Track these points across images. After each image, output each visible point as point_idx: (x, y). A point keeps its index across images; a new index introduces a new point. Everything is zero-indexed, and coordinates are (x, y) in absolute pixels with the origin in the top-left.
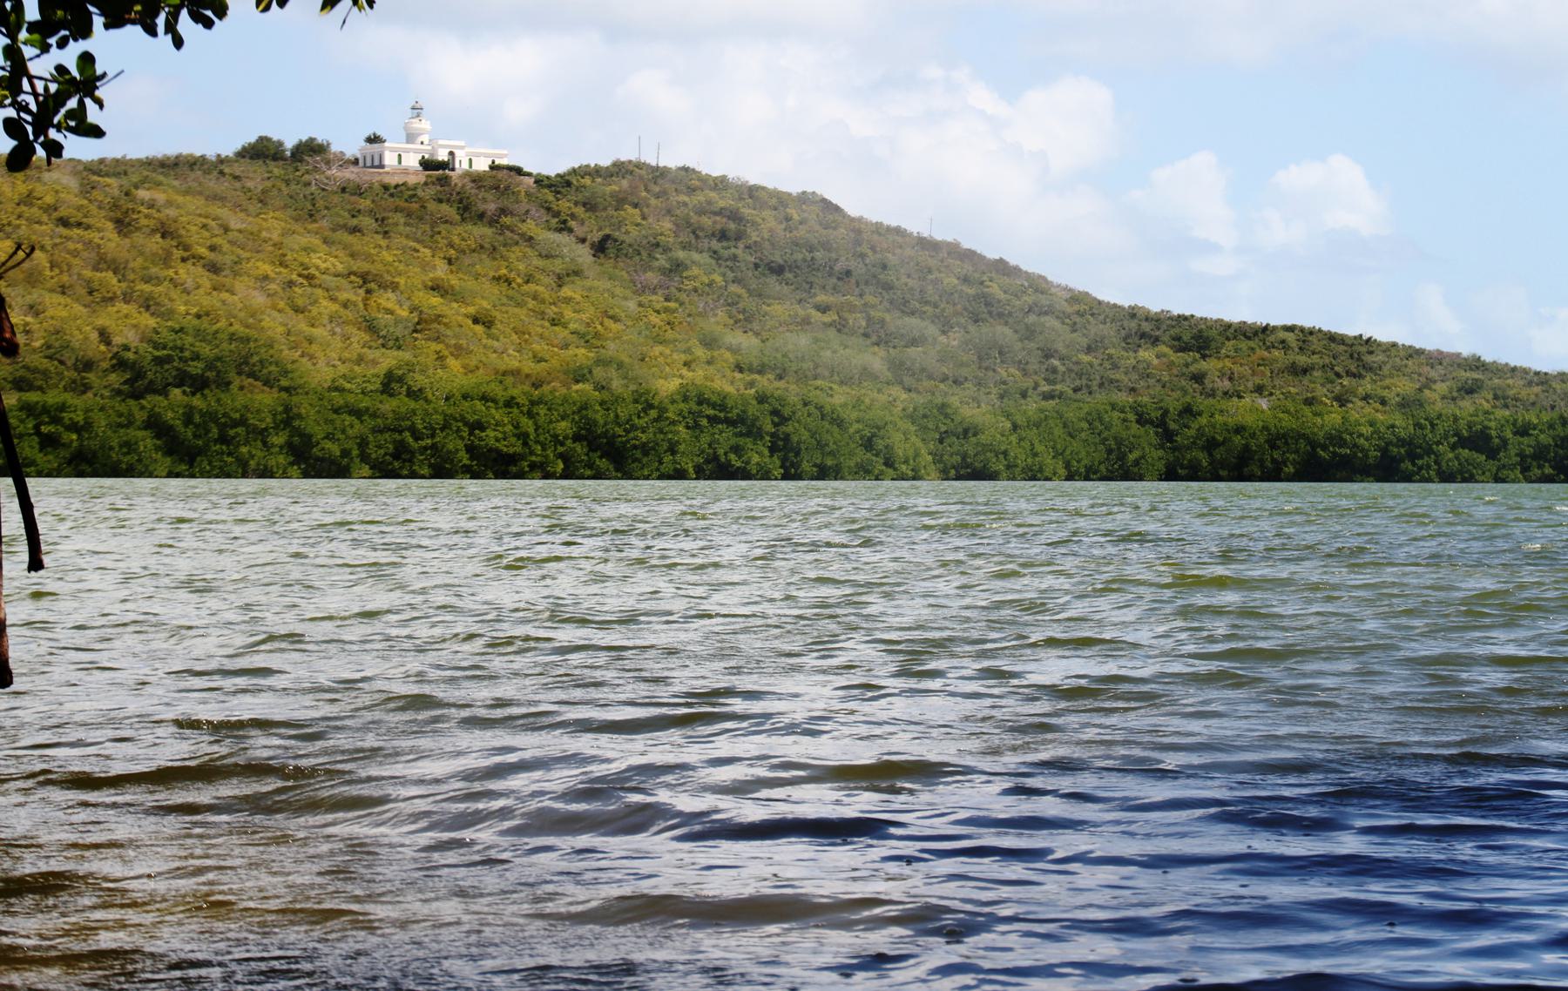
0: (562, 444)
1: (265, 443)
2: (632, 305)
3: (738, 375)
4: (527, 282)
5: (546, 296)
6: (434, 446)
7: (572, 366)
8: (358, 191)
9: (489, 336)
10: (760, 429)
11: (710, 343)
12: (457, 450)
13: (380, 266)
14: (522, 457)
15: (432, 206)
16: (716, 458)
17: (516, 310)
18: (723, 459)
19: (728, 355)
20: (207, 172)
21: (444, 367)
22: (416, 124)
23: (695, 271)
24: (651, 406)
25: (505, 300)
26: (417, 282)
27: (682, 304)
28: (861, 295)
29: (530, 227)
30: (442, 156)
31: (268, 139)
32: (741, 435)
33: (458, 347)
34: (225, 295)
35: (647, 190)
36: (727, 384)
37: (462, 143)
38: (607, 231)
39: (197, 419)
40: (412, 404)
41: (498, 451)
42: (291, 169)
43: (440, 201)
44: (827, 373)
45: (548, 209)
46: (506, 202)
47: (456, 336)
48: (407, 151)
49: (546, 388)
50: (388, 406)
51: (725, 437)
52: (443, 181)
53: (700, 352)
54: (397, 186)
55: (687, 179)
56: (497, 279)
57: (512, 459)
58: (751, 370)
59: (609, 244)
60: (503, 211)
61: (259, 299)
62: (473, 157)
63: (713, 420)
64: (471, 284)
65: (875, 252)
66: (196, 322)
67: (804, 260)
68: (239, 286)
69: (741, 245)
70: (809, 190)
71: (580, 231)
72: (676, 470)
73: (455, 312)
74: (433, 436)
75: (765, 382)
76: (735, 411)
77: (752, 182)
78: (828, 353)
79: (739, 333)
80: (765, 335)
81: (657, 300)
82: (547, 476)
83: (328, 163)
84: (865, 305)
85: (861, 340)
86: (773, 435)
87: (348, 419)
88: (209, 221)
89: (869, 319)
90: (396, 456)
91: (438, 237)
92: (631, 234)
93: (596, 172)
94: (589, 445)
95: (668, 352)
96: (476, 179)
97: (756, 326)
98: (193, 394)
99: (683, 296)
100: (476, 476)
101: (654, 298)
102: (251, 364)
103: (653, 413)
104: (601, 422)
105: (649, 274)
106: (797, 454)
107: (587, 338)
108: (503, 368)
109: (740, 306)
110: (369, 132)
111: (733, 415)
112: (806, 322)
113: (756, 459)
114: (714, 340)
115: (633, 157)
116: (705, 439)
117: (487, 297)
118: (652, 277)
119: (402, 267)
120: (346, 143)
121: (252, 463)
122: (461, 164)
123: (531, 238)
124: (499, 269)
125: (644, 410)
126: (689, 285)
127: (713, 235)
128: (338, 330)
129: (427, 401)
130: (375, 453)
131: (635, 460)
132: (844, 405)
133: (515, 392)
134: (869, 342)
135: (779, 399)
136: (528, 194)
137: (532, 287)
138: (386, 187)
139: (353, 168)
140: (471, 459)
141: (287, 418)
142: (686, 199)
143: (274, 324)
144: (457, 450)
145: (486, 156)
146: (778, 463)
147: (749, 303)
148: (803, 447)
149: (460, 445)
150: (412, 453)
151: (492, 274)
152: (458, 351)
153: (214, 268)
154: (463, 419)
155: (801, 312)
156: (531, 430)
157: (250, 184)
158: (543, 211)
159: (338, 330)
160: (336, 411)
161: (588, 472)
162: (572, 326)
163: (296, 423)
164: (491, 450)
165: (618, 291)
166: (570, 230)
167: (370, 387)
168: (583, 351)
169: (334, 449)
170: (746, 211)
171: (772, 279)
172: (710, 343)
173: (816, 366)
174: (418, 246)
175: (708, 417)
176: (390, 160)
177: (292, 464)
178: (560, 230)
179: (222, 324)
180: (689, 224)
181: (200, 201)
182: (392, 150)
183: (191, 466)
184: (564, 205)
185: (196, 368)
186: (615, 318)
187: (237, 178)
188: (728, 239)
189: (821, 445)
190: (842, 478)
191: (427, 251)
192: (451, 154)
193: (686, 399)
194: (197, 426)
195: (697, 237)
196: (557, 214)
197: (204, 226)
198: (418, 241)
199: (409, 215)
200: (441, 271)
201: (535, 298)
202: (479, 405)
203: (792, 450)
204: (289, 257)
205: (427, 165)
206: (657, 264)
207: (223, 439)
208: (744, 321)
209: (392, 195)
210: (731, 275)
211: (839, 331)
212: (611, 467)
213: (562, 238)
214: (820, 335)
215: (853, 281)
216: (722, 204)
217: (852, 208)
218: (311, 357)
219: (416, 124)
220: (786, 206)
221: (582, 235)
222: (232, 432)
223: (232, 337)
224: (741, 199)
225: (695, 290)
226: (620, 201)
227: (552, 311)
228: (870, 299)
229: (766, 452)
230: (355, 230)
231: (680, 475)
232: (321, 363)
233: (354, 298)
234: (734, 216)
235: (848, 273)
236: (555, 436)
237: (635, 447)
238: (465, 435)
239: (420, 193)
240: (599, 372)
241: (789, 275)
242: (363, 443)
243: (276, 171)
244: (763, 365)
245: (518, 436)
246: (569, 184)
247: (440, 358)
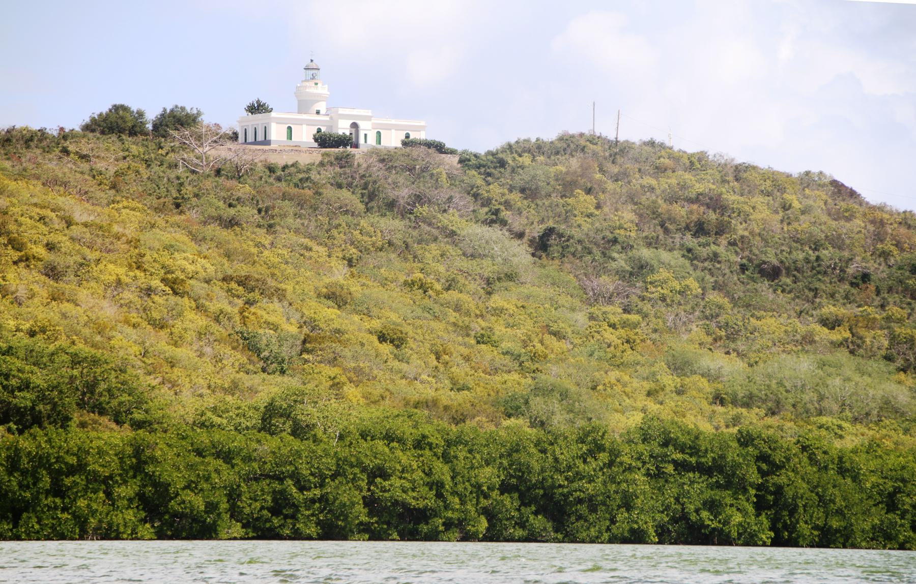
0: (486, 497)
1: (108, 494)
2: (581, 318)
3: (720, 409)
4: (448, 289)
5: (472, 306)
6: (323, 499)
7: (503, 396)
8: (238, 174)
9: (396, 357)
10: (743, 479)
11: (680, 367)
12: (353, 504)
13: (262, 269)
14: (435, 513)
15: (329, 192)
16: (684, 517)
17: (434, 324)
18: (693, 517)
19: (704, 383)
20: (47, 150)
21: (339, 397)
22: (311, 89)
23: (663, 274)
24: (601, 448)
25: (419, 312)
26: (309, 288)
27: (645, 316)
28: (883, 306)
29: (452, 219)
30: (343, 128)
31: (124, 108)
32: (718, 486)
33: (358, 371)
34: (67, 307)
35: (602, 171)
36: (704, 422)
37: (368, 113)
38: (551, 224)
39: (25, 463)
40: (296, 444)
41: (404, 505)
42: (152, 146)
43: (340, 186)
44: (836, 408)
45: (476, 196)
46: (423, 187)
47: (355, 358)
48: (300, 123)
49: (470, 424)
50: (268, 445)
51: (697, 489)
52: (344, 161)
53: (669, 380)
54: (284, 168)
55: (657, 158)
56: (410, 285)
57: (423, 515)
58: (734, 402)
59: (553, 240)
60: (419, 199)
61: (108, 311)
62: (382, 130)
63: (682, 467)
64: (377, 291)
65: (902, 250)
66: (27, 341)
67: (807, 260)
68: (83, 294)
69: (723, 241)
70: (815, 169)
71: (517, 223)
72: (632, 531)
73: (353, 324)
74: (322, 485)
75: (754, 419)
76: (710, 455)
77: (739, 160)
78: (838, 381)
79: (719, 354)
80: (753, 357)
81: (614, 312)
82: (467, 537)
83: (199, 138)
84: (888, 319)
85: (882, 365)
86: (759, 487)
87: (216, 463)
88: (48, 213)
89: (893, 338)
90: (275, 511)
91: (334, 232)
92: (581, 228)
93: (538, 149)
94: (521, 497)
95: (626, 378)
96: (386, 159)
97: (741, 345)
98: (21, 432)
99: (647, 307)
100: (376, 536)
101: (609, 308)
102: (95, 395)
103: (604, 457)
104: (537, 467)
105: (604, 279)
106: (793, 511)
107: (527, 361)
108: (415, 397)
109: (722, 319)
110: (251, 99)
111: (708, 460)
112: (808, 340)
113: (738, 518)
114: (687, 363)
115: (586, 131)
116: (671, 491)
117: (397, 307)
118: (607, 283)
119: (290, 270)
120: (221, 112)
121: (93, 522)
122: (368, 140)
123: (453, 233)
124: (411, 272)
125: (591, 452)
126: (655, 292)
127: (687, 228)
128: (208, 350)
129: (316, 440)
130: (247, 507)
131: (580, 518)
132: (855, 451)
133: (427, 429)
134: (892, 367)
135: (769, 441)
136: (450, 177)
137: (453, 295)
138: (271, 169)
139: (230, 145)
140: (370, 514)
141: (138, 462)
142: (653, 182)
143: (126, 343)
144: (353, 504)
145: (398, 128)
146: (766, 523)
147: (732, 315)
148: (800, 503)
149: (357, 497)
150: (296, 507)
151: (402, 278)
152: (359, 376)
153: (52, 272)
154: (360, 464)
155: (802, 329)
156: (447, 478)
157: (100, 165)
158: (469, 198)
159: (208, 350)
160: (199, 453)
161: (520, 533)
162: (505, 345)
163: (150, 469)
164: (396, 503)
165: (564, 300)
166: (504, 223)
167: (245, 423)
168: (515, 376)
169: (198, 502)
170: (731, 198)
171: (764, 286)
172: (680, 367)
173: (821, 398)
174: (306, 241)
175: (674, 462)
176: (277, 134)
177: (144, 521)
178: (491, 223)
179: (63, 342)
180: (655, 214)
181: (37, 187)
182: (280, 121)
183: (16, 525)
184: (495, 190)
185: (24, 399)
186: (556, 334)
187: (83, 157)
188: (706, 233)
189: (824, 502)
190: (854, 546)
191: (322, 250)
192: (355, 126)
193: (645, 439)
194: (24, 473)
195: (666, 231)
196: (487, 202)
197: (42, 219)
198: (312, 238)
199: (301, 205)
200: (339, 274)
201: (457, 308)
202: (380, 445)
203: (786, 506)
204: (148, 258)
205: (324, 140)
206: (614, 265)
207: (57, 490)
208: (727, 338)
209: (279, 179)
210: (710, 279)
211: (852, 352)
212: (549, 525)
213: (495, 233)
214: (829, 357)
215: (872, 287)
216: (700, 188)
217: (871, 194)
218: (174, 384)
219: (311, 89)
220: (782, 190)
221: (517, 227)
222: (68, 481)
223: (76, 361)
224: (724, 181)
225: (663, 299)
226: (568, 186)
227: (478, 325)
228: (894, 310)
229: (751, 509)
230: (231, 223)
231: (637, 537)
232: (186, 395)
233: (228, 309)
234: (715, 203)
235: (865, 277)
236: (478, 486)
237: (580, 501)
238: (363, 484)
239: (314, 175)
240: (538, 405)
241: (786, 280)
242: (233, 495)
243: (134, 149)
244: (751, 396)
245: (430, 486)
246: (502, 164)
247: (336, 385)
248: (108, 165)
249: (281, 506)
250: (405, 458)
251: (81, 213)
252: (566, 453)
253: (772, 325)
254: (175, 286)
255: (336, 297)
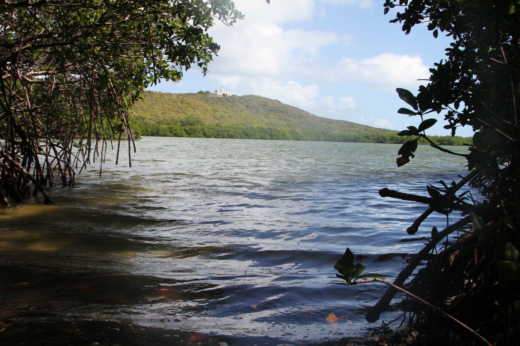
8: (214, 98)
11: (262, 120)
29: (237, 104)
36: (264, 126)
50: (216, 128)
51: (263, 134)
52: (225, 97)
53: (260, 122)
55: (259, 97)
57: (233, 136)
61: (200, 113)
62: (229, 94)
73: (226, 115)
75: (269, 126)
81: (255, 114)
93: (247, 96)
96: (230, 97)
100: (228, 138)
112: (275, 118)
118: (254, 111)
120: (212, 92)
122: (228, 94)
130: (214, 135)
152: (227, 121)
153: (194, 109)
169: (209, 134)
172: (262, 120)
176: (218, 94)
184: (242, 101)
185: (191, 122)
189: (276, 135)
200: (225, 109)
205: (223, 95)
208: (267, 117)
226: (250, 100)
231: (257, 139)
234: (266, 103)
242: (213, 133)
248: (200, 97)
249: (218, 135)
250: (231, 130)
251: (197, 102)
252: (249, 130)
253: (272, 116)
254: (207, 110)
255: (224, 112)
